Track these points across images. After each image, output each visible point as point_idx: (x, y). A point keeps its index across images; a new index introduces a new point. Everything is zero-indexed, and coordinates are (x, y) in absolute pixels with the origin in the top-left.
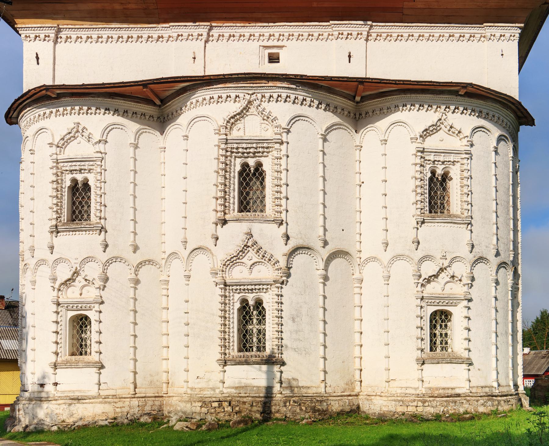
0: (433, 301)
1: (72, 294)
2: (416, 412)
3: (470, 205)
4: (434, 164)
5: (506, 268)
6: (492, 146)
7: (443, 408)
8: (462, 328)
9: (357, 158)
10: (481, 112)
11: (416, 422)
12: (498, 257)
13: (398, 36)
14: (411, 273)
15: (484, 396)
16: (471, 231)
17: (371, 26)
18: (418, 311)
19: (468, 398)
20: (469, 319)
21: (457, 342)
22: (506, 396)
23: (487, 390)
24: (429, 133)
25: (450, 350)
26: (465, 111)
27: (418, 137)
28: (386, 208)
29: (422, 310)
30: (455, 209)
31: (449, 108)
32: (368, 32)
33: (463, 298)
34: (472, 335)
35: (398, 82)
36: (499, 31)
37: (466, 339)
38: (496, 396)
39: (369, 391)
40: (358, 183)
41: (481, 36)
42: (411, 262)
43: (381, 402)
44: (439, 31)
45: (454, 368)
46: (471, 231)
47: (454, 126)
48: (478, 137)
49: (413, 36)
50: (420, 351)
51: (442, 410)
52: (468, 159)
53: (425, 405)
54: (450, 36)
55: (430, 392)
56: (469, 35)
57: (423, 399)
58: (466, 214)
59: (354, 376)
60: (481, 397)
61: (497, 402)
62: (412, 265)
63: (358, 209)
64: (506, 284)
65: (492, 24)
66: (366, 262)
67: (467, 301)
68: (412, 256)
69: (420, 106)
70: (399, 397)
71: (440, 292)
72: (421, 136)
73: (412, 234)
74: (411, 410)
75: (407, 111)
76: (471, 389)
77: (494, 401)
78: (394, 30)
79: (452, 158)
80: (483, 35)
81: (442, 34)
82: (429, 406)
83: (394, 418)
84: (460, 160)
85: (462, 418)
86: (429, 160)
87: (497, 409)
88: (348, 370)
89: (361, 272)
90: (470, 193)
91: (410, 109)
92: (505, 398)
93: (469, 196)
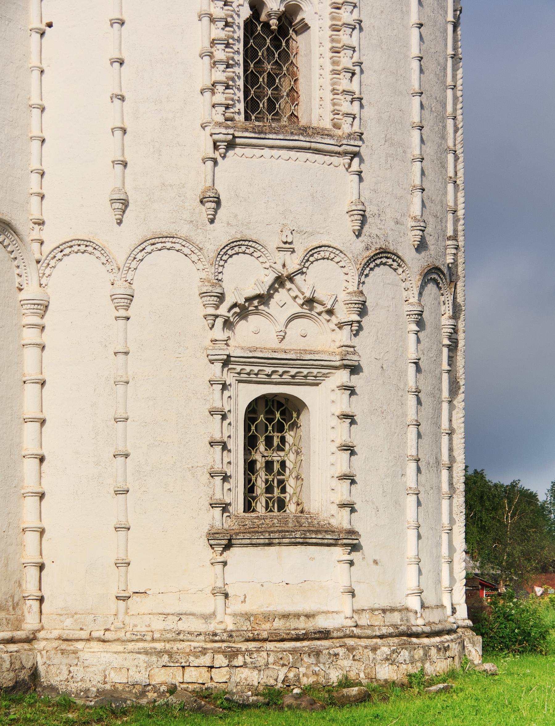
0: (256, 369)
2: (209, 685)
3: (356, 104)
5: (438, 284)
7: (285, 670)
8: (333, 448)
11: (213, 713)
12: (423, 254)
15: (391, 635)
16: (359, 173)
18: (216, 399)
19: (350, 642)
21: (318, 488)
22: (438, 633)
23: (396, 618)
25: (291, 508)
28: (122, 98)
30: (316, 113)
33: (338, 364)
34: (358, 465)
37: (343, 477)
38: (417, 635)
39: (69, 628)
40: (35, 24)
42: (194, 258)
43: (106, 658)
45: (312, 559)
46: (359, 173)
50: (218, 511)
51: (281, 677)
53: (235, 663)
55: (246, 626)
57: (229, 646)
58: (346, 128)
59: (20, 585)
60: (381, 637)
61: (421, 652)
62: (200, 266)
63: (35, 100)
64: (438, 328)
66: (59, 256)
68: (198, 239)
70: (158, 640)
71: (274, 343)
73: (198, 178)
74: (195, 676)
76: (356, 617)
77: (415, 647)
82: (245, 665)
83: (144, 701)
85: (339, 699)
87: (422, 669)
88: (6, 565)
89: (44, 281)
90: (357, 69)
92: (437, 639)
93: (356, 78)
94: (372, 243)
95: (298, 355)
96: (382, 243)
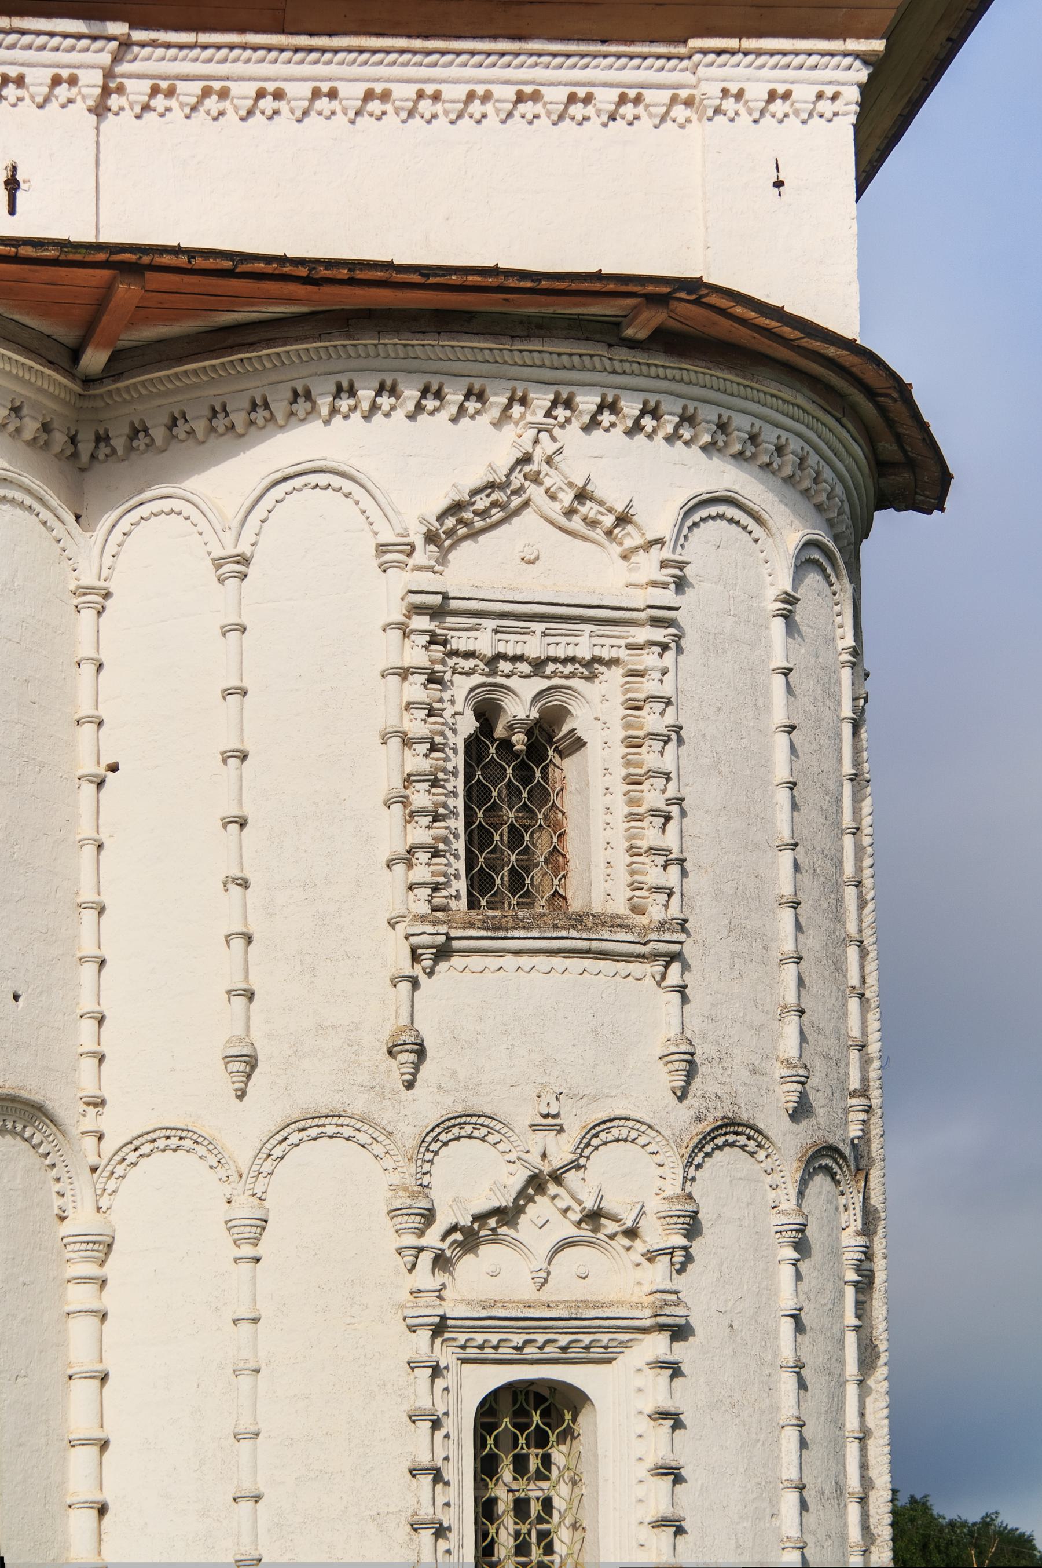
0: (494, 1339)
1: (490, 1278)
3: (674, 870)
4: (493, 673)
5: (833, 1176)
6: (772, 592)
9: (86, 651)
10: (722, 427)
12: (804, 1123)
13: (261, 94)
14: (380, 1200)
16: (682, 990)
17: (126, 44)
18: (421, 1393)
20: (677, 1422)
24: (466, 524)
26: (648, 422)
27: (419, 541)
29: (440, 1384)
31: (568, 404)
32: (109, 74)
33: (647, 1323)
34: (689, 1501)
35: (324, 272)
36: (765, 72)
37: (661, 1523)
40: (89, 767)
41: (674, 99)
42: (378, 1149)
44: (469, 72)
46: (682, 990)
47: (598, 488)
48: (710, 547)
49: (333, 94)
52: (665, 647)
54: (520, 98)
56: (614, 94)
58: (656, 912)
63: (87, 895)
64: (836, 1252)
65: (732, 43)
66: (132, 1157)
67: (666, 1335)
68: (386, 1116)
69: (425, 392)
71: (527, 1291)
72: (431, 538)
73: (384, 1012)
75: (356, 416)
78: (239, 68)
79: (584, 644)
80: (684, 93)
81: (480, 90)
84: (623, 654)
86: (469, 655)
89: (104, 1203)
90: (675, 810)
91: (374, 407)
93: (672, 826)
94: (707, 1109)
95: (573, 1311)
96: (726, 1109)
